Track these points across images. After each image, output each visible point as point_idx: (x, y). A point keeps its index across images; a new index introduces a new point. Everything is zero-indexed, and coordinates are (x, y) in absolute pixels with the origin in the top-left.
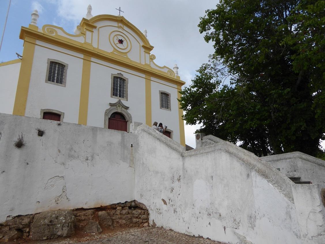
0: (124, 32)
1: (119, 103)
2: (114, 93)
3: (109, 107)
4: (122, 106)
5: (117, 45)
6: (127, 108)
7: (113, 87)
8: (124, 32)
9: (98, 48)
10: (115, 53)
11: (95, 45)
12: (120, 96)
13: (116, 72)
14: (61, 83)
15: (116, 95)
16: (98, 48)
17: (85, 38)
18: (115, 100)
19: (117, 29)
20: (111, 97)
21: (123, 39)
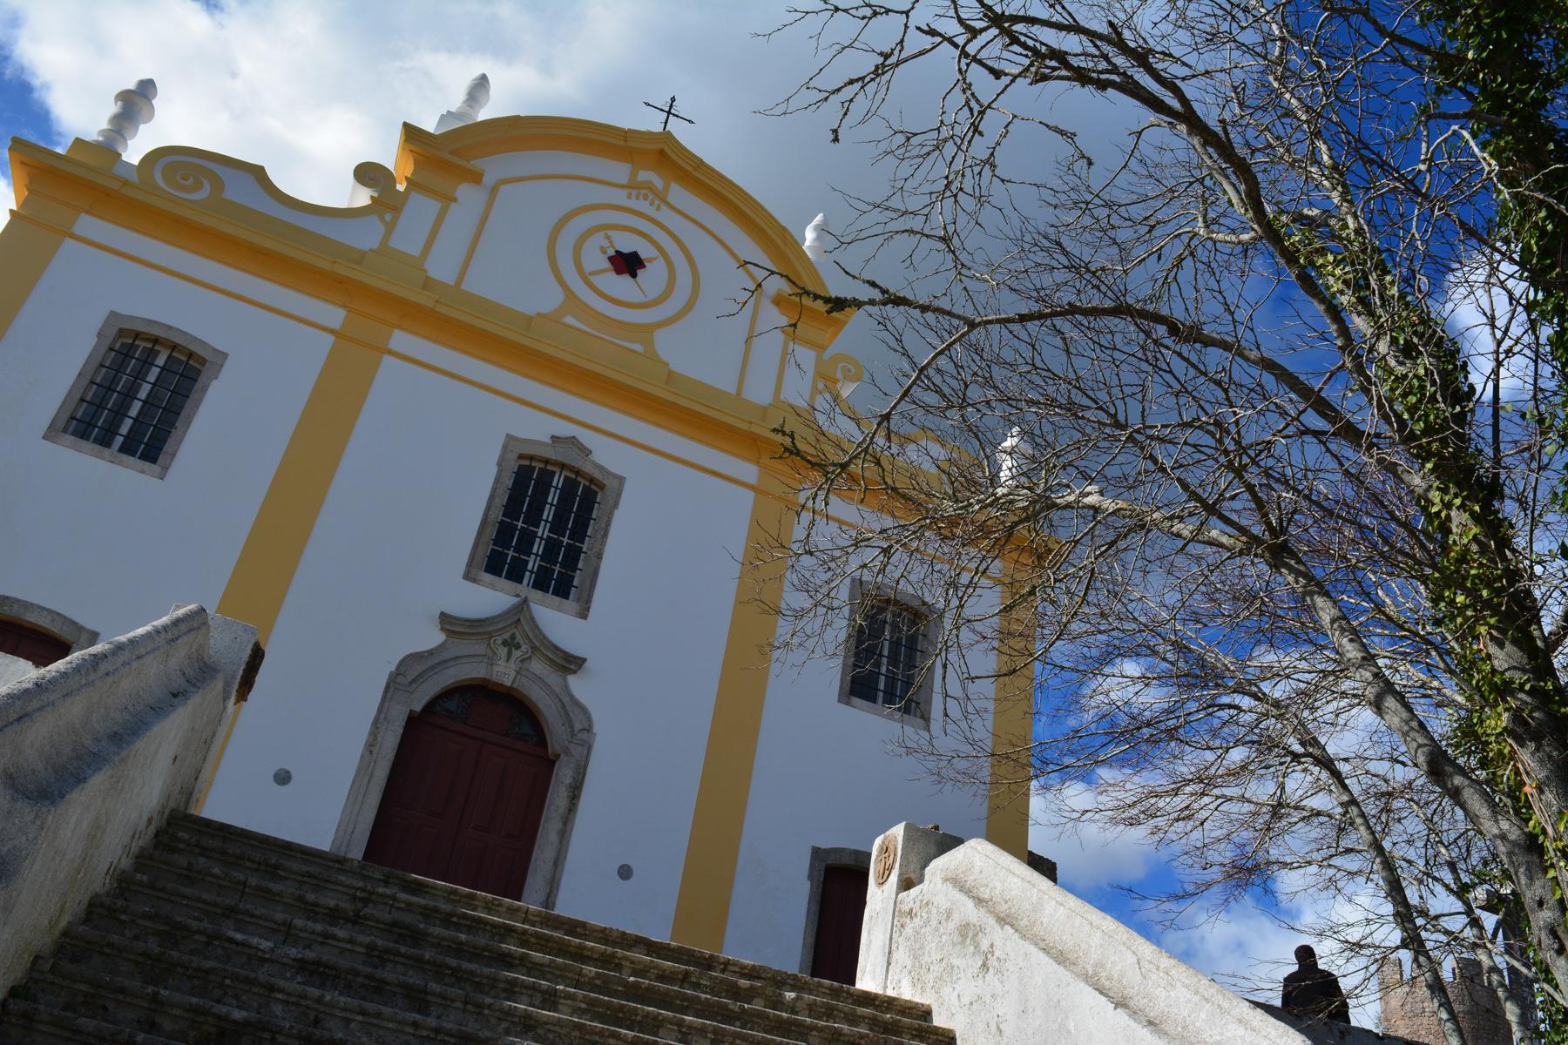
0: (665, 215)
1: (514, 629)
2: (500, 554)
3: (434, 638)
4: (534, 648)
5: (598, 281)
6: (570, 663)
7: (497, 514)
8: (665, 215)
9: (739, 394)
10: (569, 320)
11: (442, 267)
12: (541, 584)
13: (538, 430)
14: (154, 460)
15: (516, 575)
16: (739, 394)
17: (390, 228)
18: (489, 599)
19: (620, 197)
20: (467, 576)
21: (645, 251)
